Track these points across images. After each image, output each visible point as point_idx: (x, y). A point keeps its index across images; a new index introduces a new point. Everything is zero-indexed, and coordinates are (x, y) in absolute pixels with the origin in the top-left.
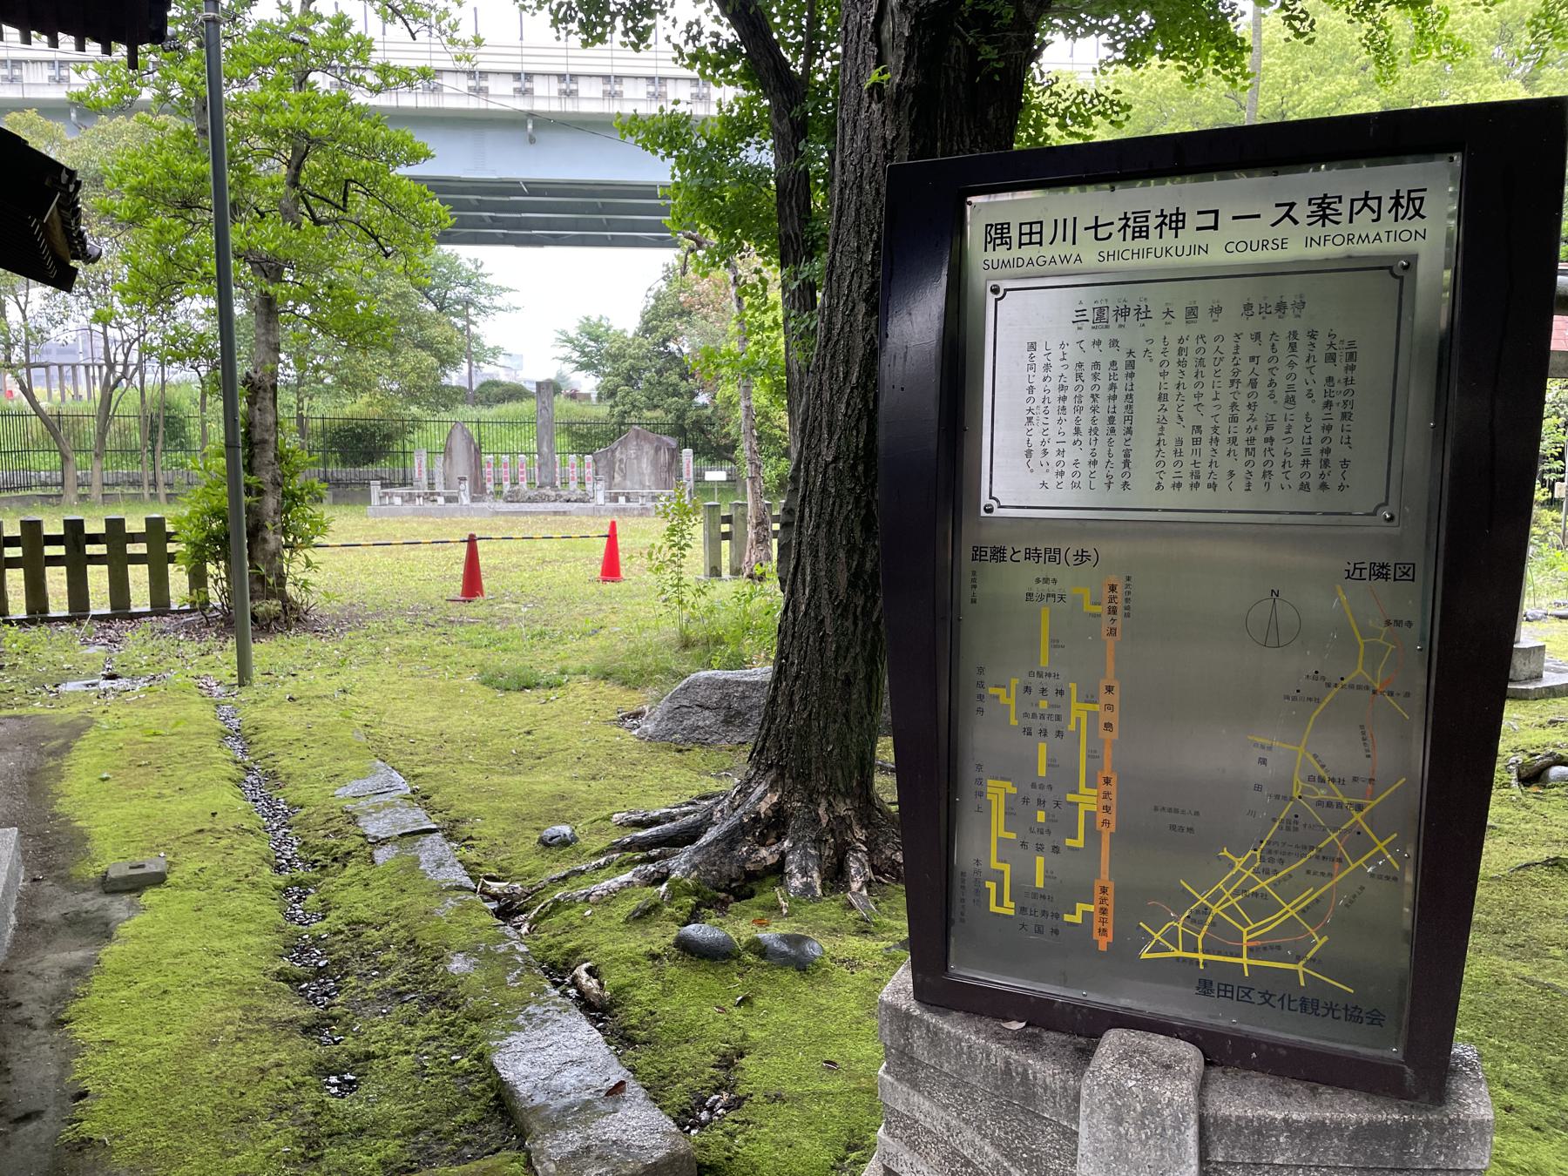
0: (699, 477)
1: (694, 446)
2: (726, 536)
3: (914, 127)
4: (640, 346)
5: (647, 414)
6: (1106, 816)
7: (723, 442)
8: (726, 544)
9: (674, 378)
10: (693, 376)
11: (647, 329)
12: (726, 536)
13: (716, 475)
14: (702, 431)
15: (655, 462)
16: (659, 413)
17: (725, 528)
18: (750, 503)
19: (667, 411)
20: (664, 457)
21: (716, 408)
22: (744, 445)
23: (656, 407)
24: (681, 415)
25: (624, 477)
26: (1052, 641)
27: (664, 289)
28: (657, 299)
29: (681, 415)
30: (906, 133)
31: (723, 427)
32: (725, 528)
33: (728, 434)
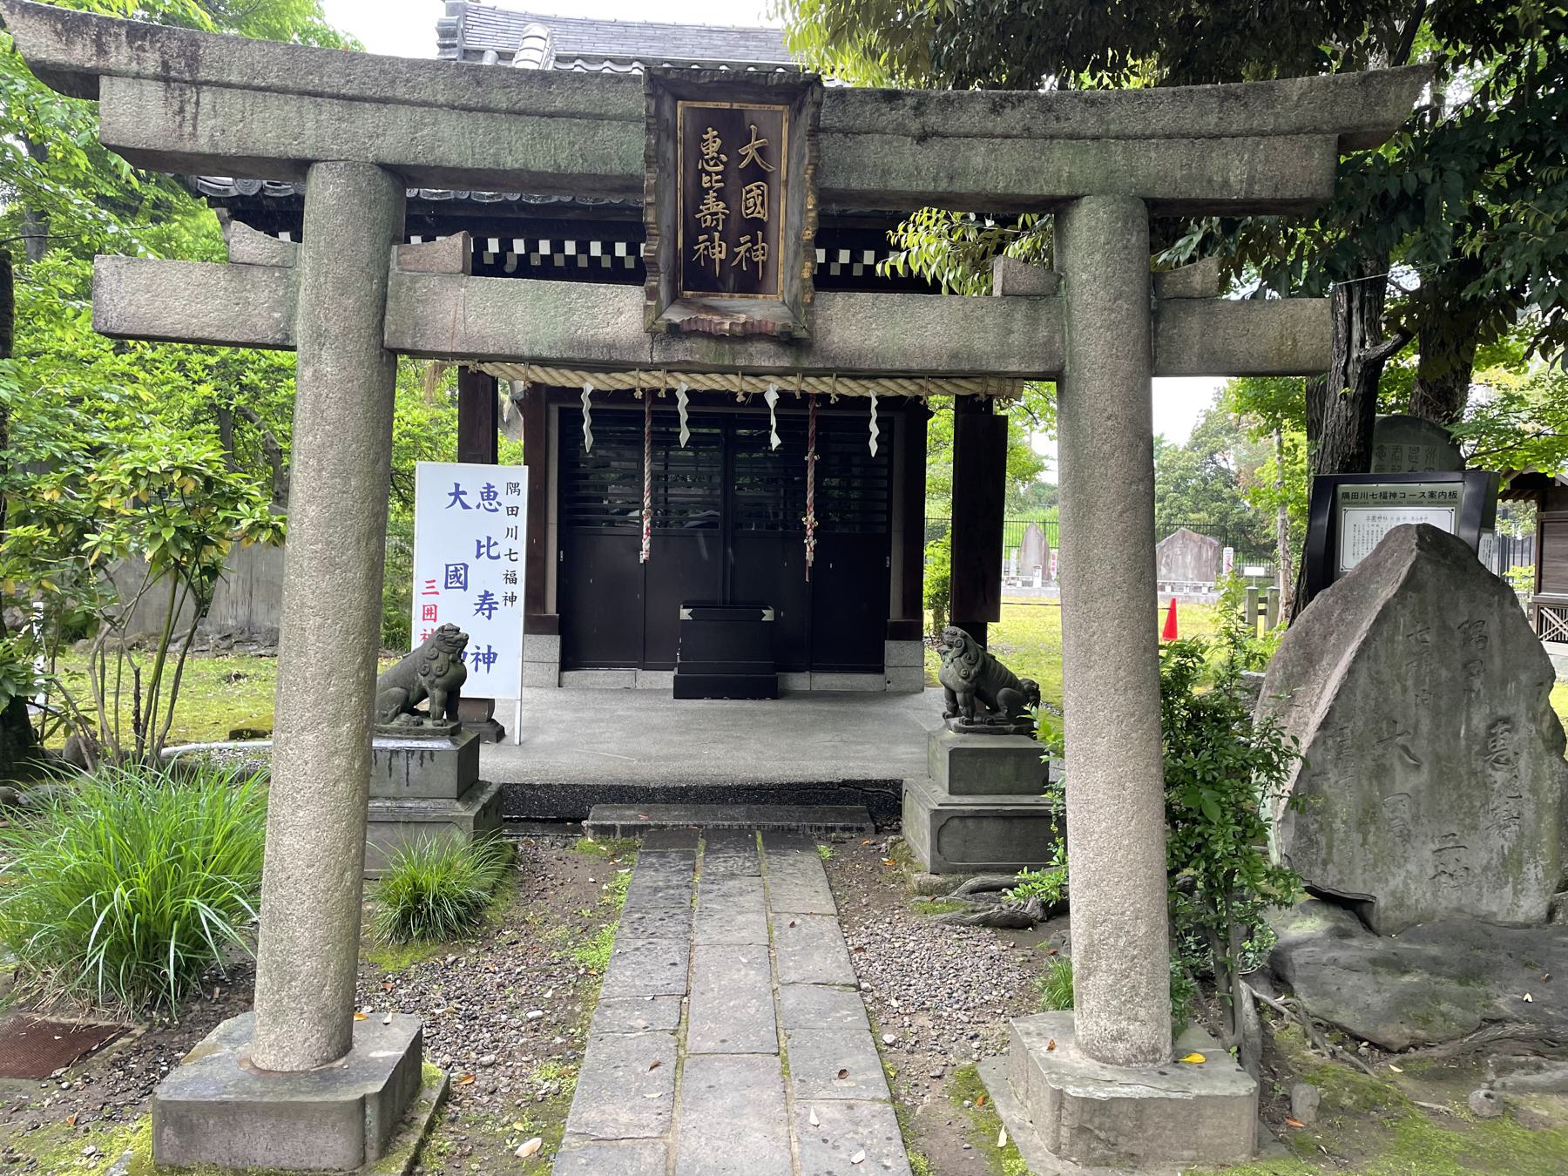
0: (1238, 573)
1: (1234, 545)
2: (1262, 612)
3: (1362, 411)
4: (1190, 458)
5: (1192, 516)
6: (510, 588)
7: (1263, 541)
8: (1261, 618)
9: (1219, 486)
10: (1236, 483)
11: (1196, 443)
12: (1262, 612)
13: (1255, 570)
14: (1243, 532)
15: (1198, 557)
16: (1204, 515)
17: (1261, 606)
18: (1282, 588)
19: (1211, 514)
20: (1208, 553)
21: (1257, 511)
22: (1280, 547)
23: (1200, 510)
24: (1224, 517)
25: (1170, 570)
26: (432, 753)
27: (1214, 409)
28: (1208, 418)
29: (1224, 517)
30: (1357, 414)
31: (1263, 528)
32: (1261, 606)
33: (1268, 535)
